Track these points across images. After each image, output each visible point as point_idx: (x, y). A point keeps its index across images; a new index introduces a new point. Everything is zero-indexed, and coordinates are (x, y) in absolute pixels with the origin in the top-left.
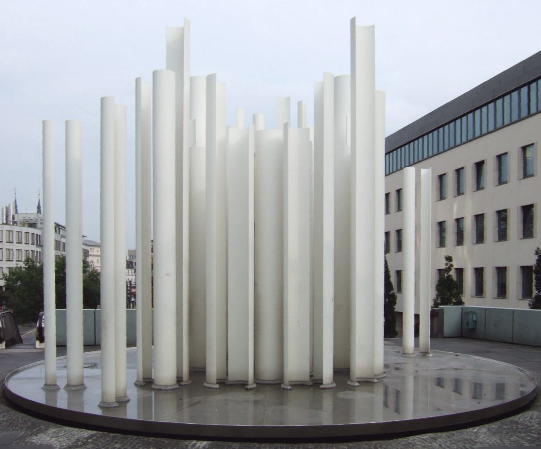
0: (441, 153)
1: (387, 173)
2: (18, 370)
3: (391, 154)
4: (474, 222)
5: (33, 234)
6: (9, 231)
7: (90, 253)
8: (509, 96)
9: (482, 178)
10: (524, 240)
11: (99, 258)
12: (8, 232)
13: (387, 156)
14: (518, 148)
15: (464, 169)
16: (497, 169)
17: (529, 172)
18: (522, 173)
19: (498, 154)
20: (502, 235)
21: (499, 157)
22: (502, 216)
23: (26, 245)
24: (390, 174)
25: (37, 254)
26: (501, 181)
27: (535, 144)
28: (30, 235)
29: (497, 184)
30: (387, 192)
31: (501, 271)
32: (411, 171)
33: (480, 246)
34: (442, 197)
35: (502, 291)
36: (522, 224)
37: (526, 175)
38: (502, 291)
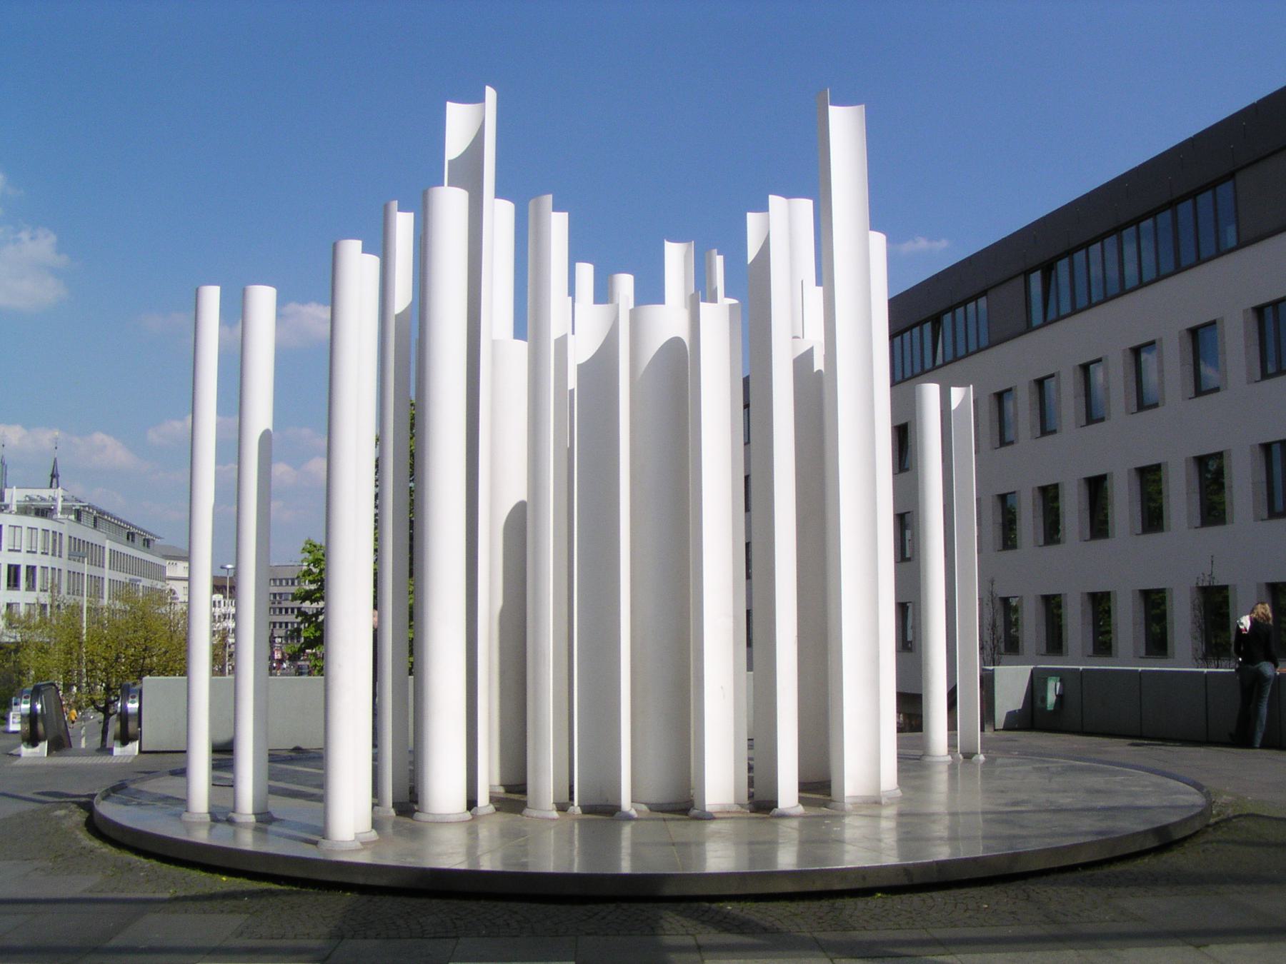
0: (1064, 317)
1: (899, 377)
2: (802, 363)
3: (907, 335)
4: (1040, 503)
5: (45, 531)
6: (15, 527)
7: (168, 574)
8: (1209, 194)
9: (908, 456)
10: (1004, 552)
11: (186, 584)
12: (30, 530)
13: (898, 339)
14: (1124, 350)
15: (1218, 325)
16: (1083, 392)
17: (1049, 428)
18: (1135, 401)
19: (998, 390)
20: (1052, 532)
21: (1040, 383)
22: (1096, 487)
23: (30, 555)
24: (904, 380)
25: (53, 574)
26: (1046, 429)
27: (1157, 342)
28: (40, 533)
29: (1084, 422)
30: (903, 422)
31: (1052, 604)
32: (931, 392)
33: (1053, 549)
34: (1003, 442)
35: (1157, 644)
36: (1088, 513)
37: (1045, 431)
38: (1157, 644)
